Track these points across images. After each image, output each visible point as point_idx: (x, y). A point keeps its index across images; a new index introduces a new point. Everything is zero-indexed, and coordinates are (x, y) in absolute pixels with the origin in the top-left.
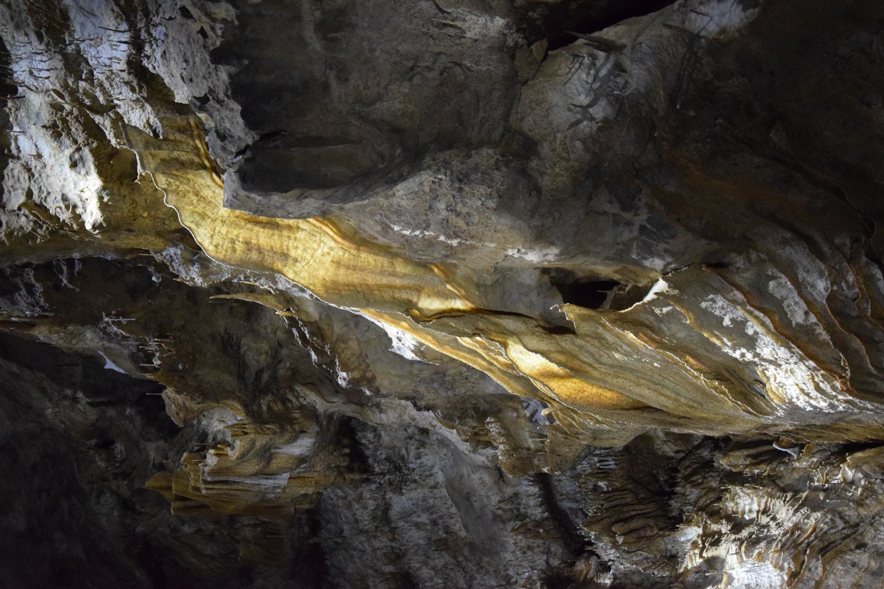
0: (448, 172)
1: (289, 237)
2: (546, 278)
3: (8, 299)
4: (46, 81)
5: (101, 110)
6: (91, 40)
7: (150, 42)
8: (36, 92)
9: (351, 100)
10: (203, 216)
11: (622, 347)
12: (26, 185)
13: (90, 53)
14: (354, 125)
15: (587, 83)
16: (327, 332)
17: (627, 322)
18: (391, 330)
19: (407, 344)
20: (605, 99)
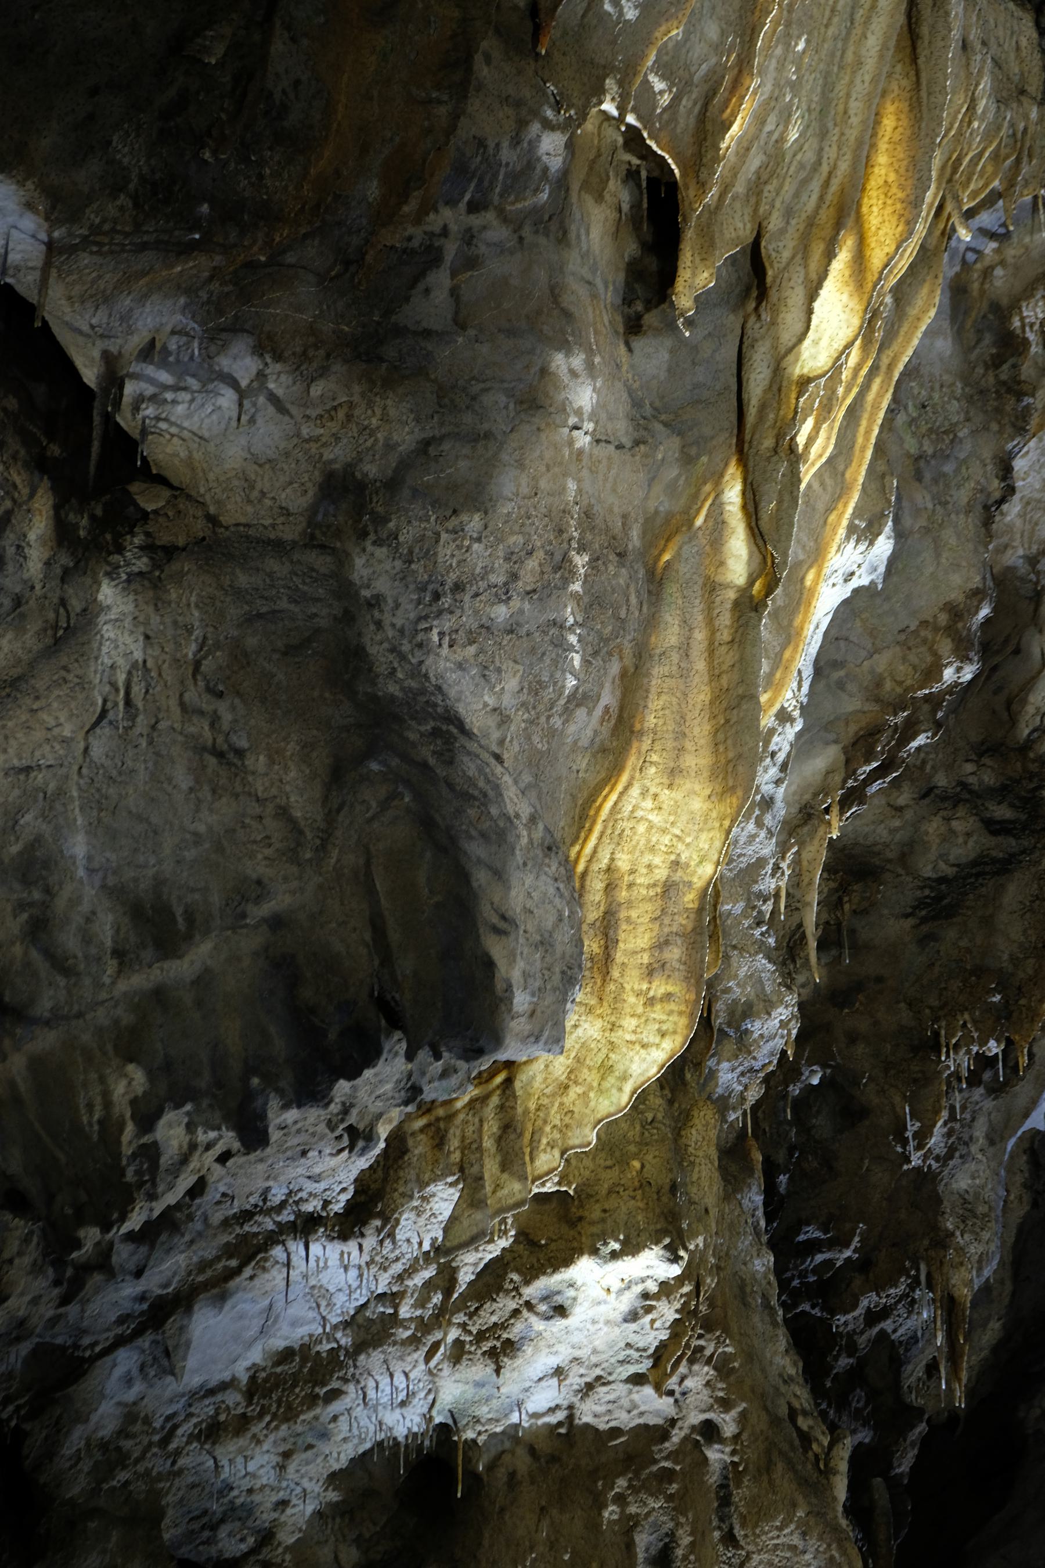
0: (424, 625)
1: (631, 885)
2: (651, 319)
3: (907, 1350)
4: (412, 1376)
5: (447, 1278)
6: (318, 1306)
7: (297, 1203)
8: (437, 1392)
9: (294, 869)
10: (606, 1069)
11: (770, 133)
12: (620, 1389)
13: (344, 1305)
14: (338, 861)
15: (192, 400)
16: (863, 724)
17: (699, 155)
18: (827, 599)
19: (859, 559)
20: (216, 359)
